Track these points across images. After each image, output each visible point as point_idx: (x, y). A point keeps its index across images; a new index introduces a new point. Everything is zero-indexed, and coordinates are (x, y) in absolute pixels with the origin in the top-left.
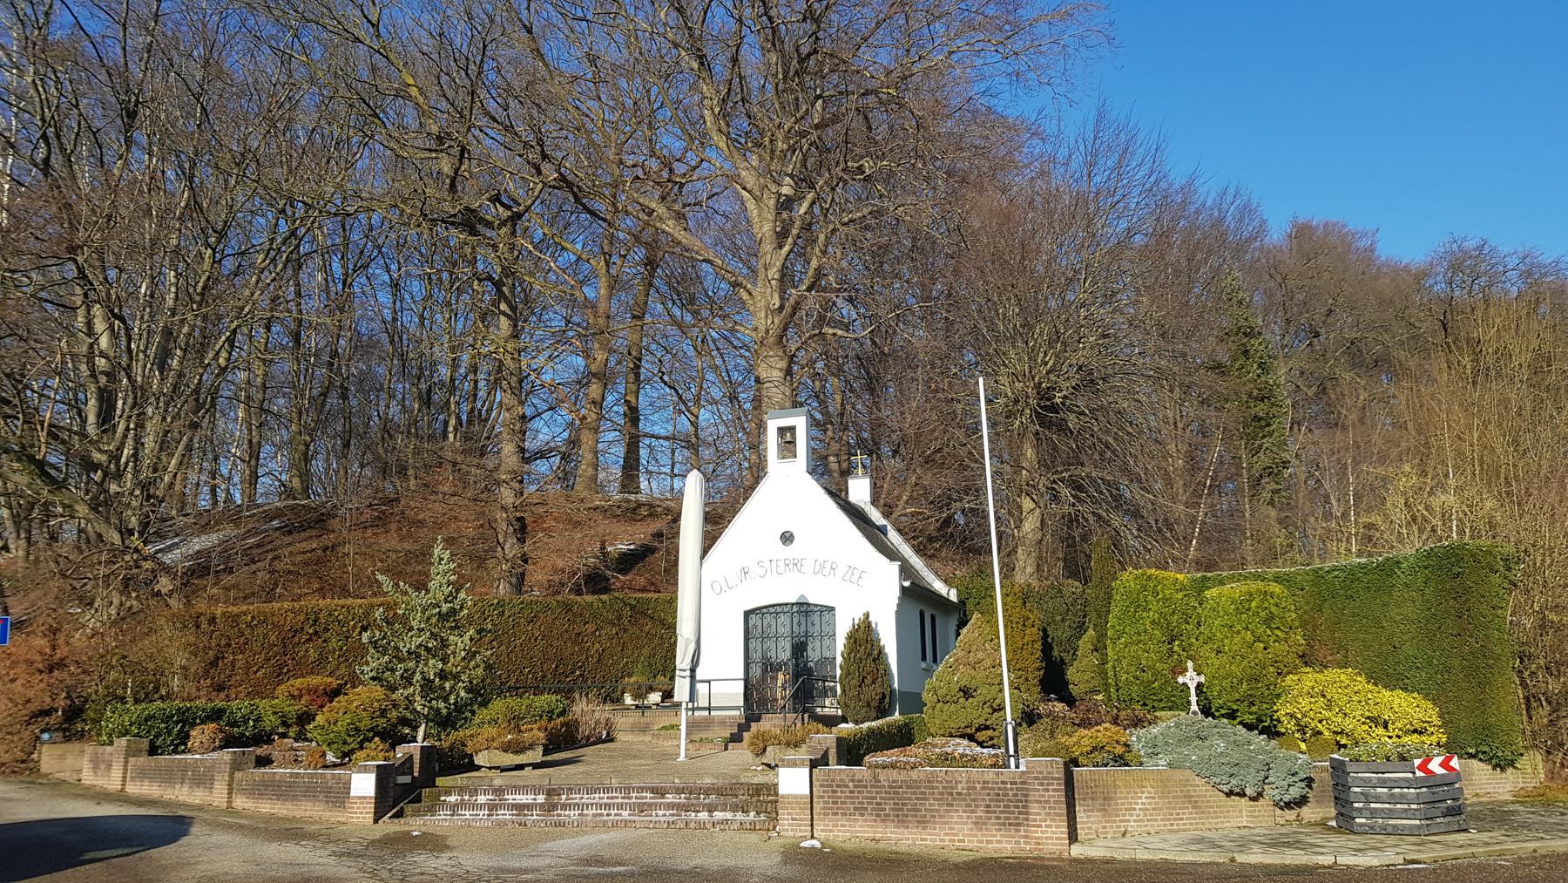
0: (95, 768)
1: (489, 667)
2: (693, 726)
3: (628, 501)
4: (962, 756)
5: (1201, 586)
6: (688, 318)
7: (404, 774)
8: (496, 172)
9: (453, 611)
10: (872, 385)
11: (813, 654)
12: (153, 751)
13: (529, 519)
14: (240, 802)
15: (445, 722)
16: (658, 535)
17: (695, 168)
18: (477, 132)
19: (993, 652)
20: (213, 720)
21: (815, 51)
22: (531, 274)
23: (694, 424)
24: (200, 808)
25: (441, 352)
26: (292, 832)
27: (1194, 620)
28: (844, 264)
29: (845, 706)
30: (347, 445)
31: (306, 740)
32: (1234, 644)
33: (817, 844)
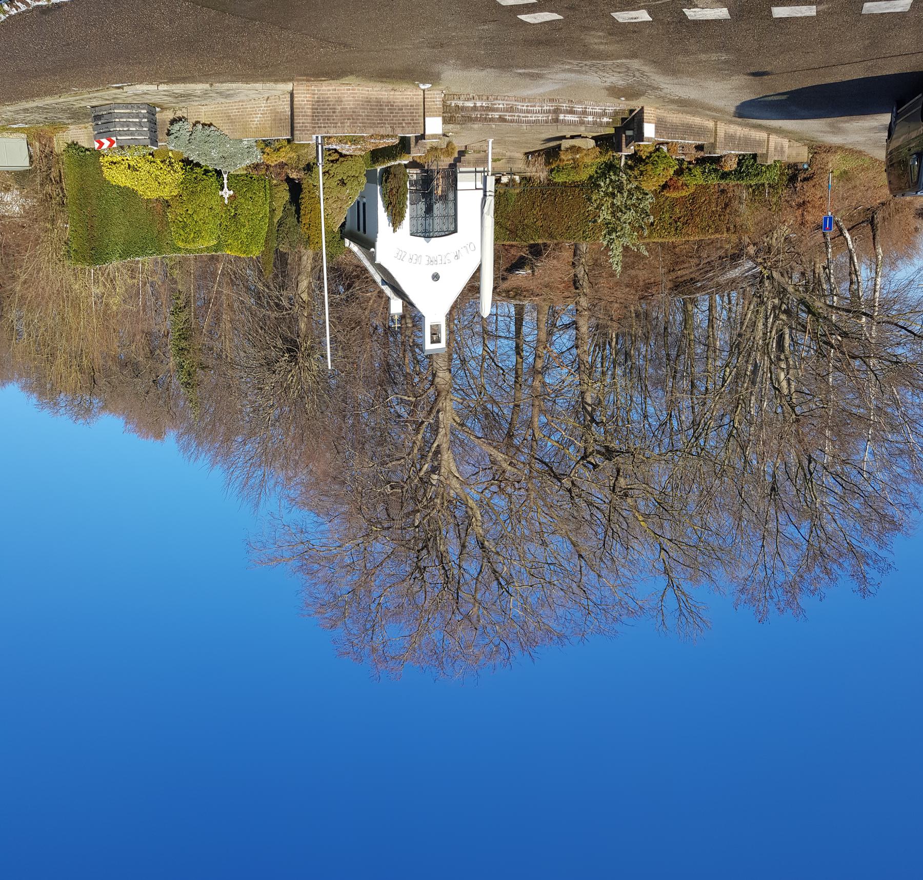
0: (782, 148)
1: (589, 199)
2: (484, 161)
3: (520, 300)
4: (346, 143)
5: (217, 247)
6: (489, 406)
7: (630, 136)
8: (596, 481)
9: (609, 233)
10: (387, 368)
11: (422, 206)
12: (755, 156)
13: (572, 289)
14: (710, 124)
15: (610, 167)
16: (504, 279)
17: (486, 489)
18: (607, 501)
19: (328, 208)
20: (725, 173)
21: (419, 551)
22: (575, 427)
23: (485, 345)
24: (731, 122)
25: (621, 382)
26: (684, 104)
27: (223, 227)
28: (403, 436)
29: (405, 174)
30: (666, 328)
31: (678, 160)
32: (203, 213)
33: (422, 87)
